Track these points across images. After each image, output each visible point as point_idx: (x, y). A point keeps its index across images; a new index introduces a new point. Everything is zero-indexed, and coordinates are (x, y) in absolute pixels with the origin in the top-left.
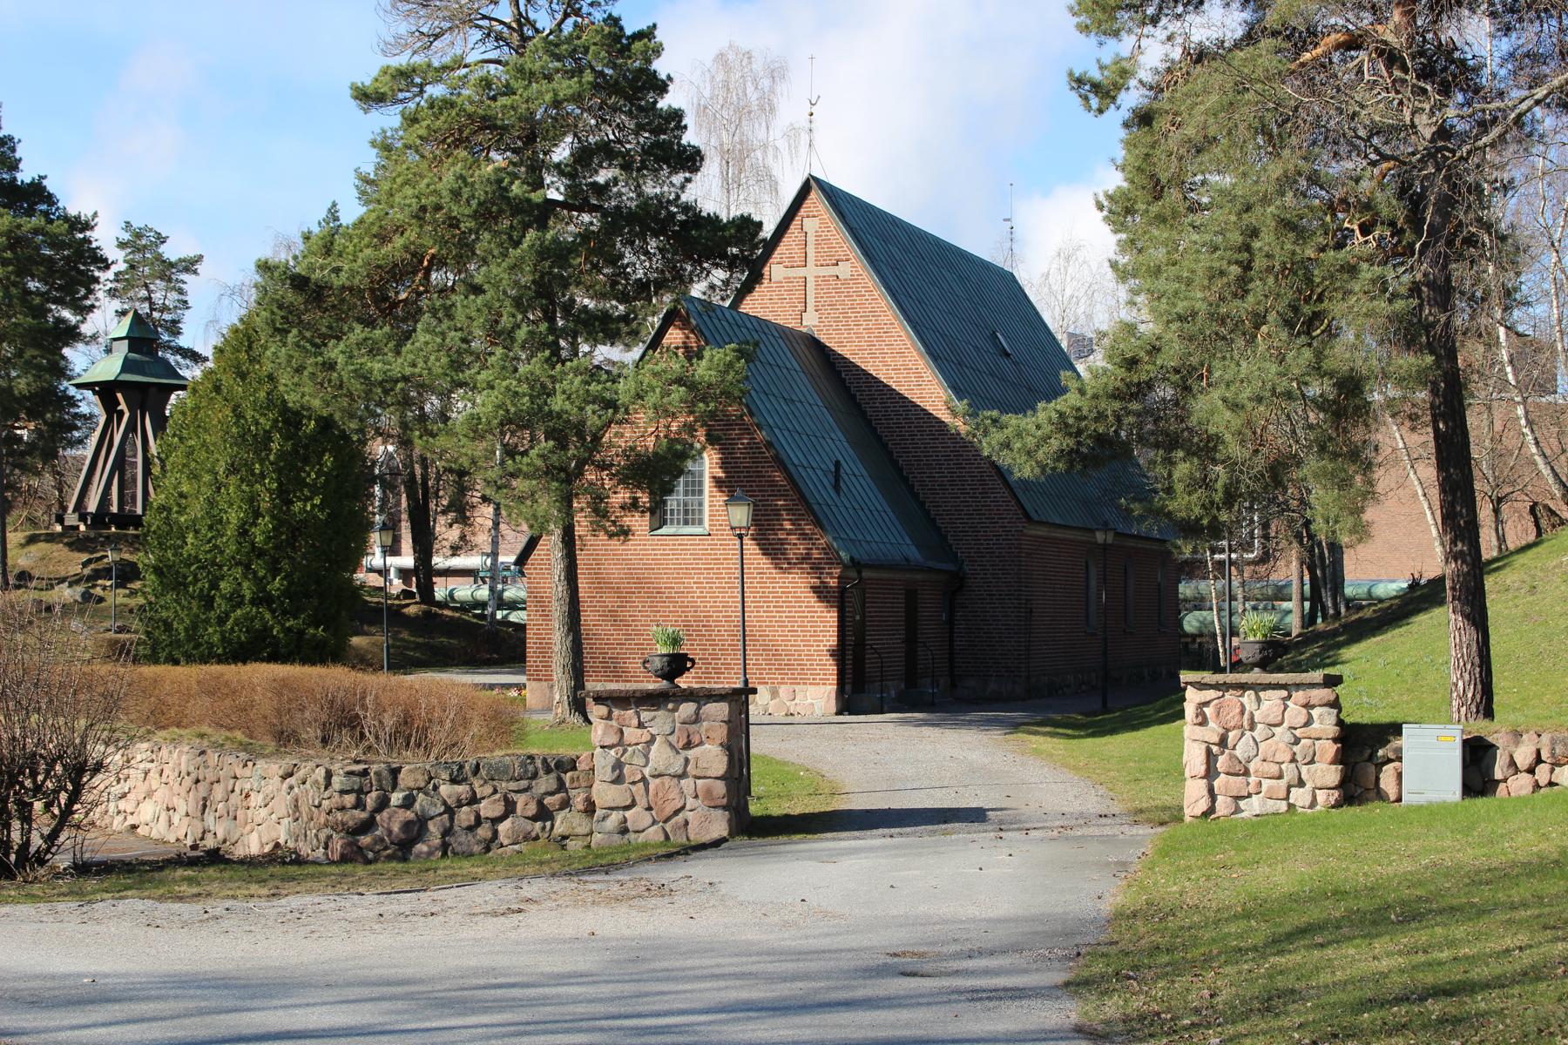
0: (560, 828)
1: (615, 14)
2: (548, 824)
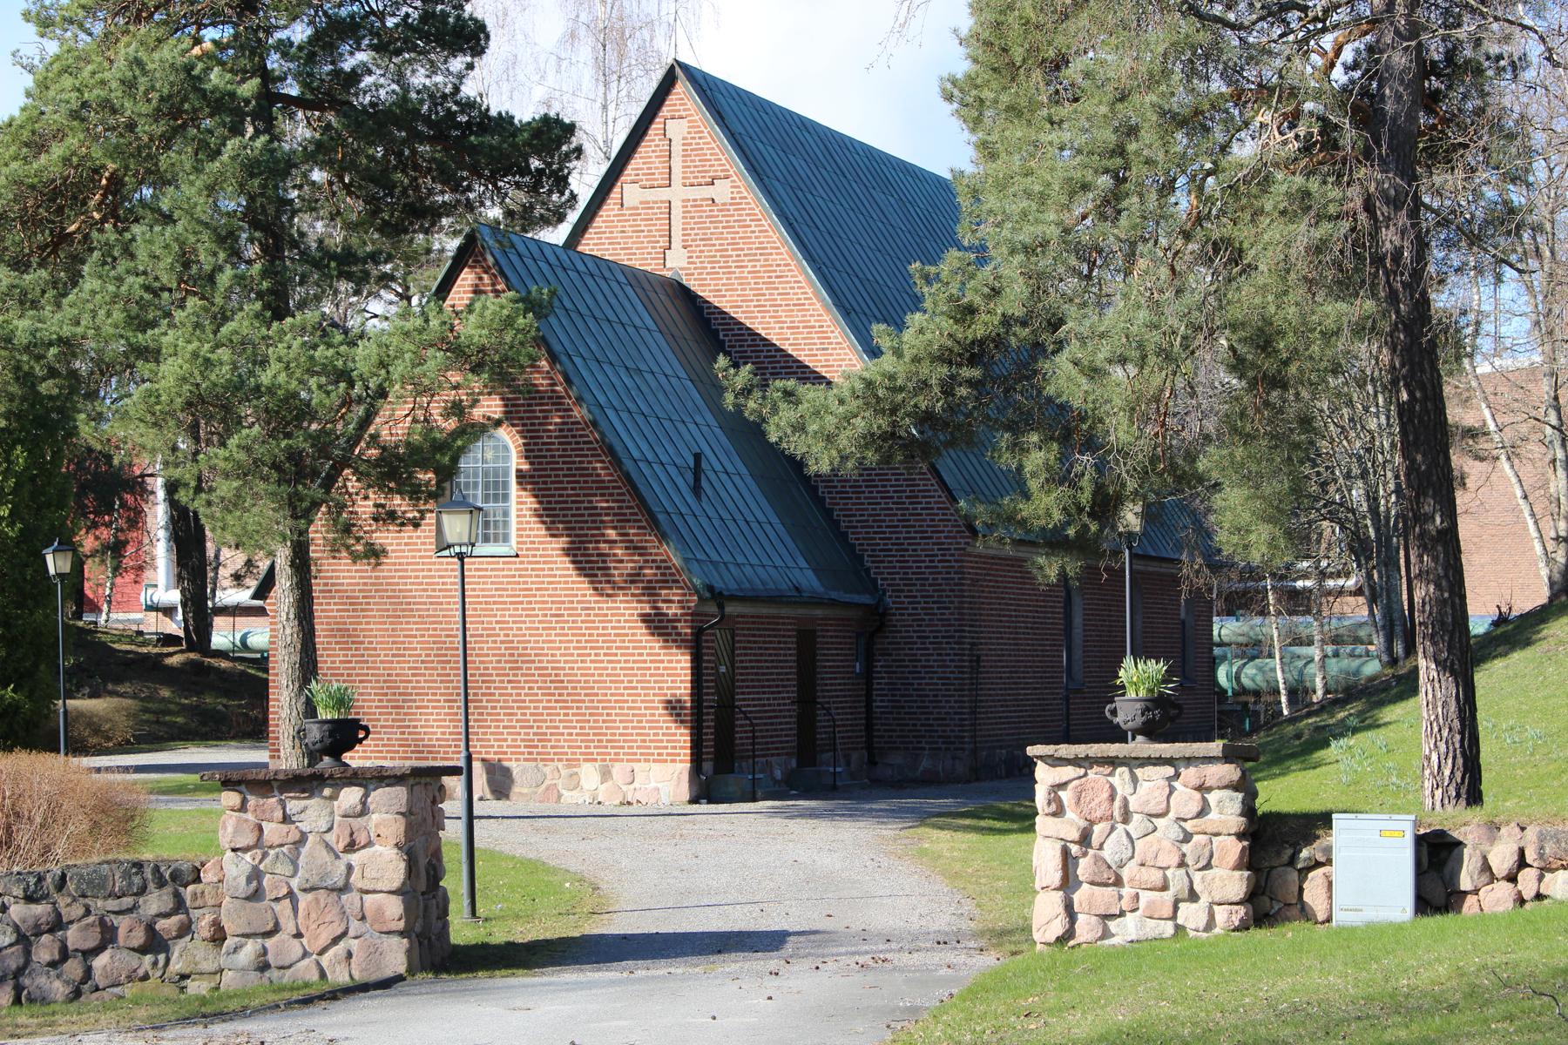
0: (176, 966)
2: (162, 957)
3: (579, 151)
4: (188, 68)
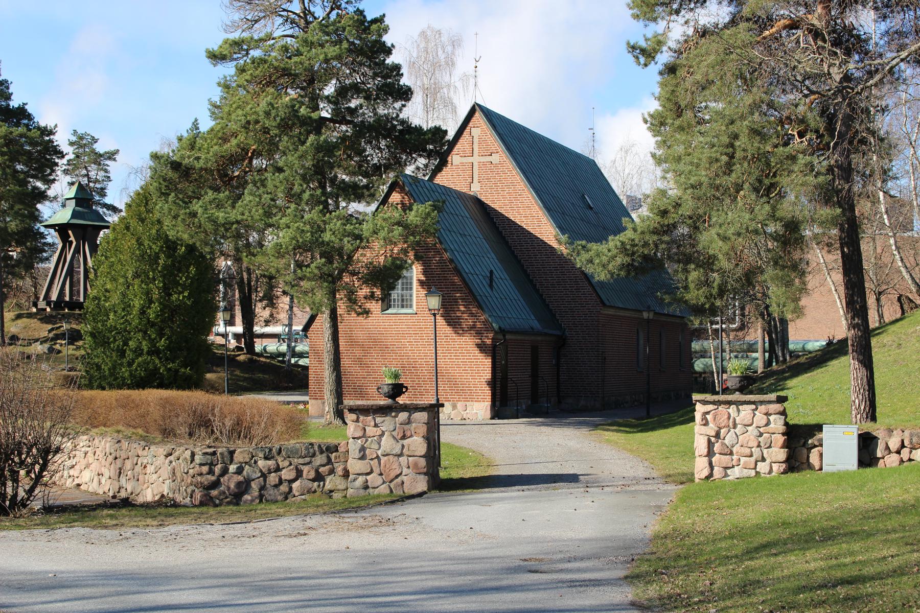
1: (361, 8)
2: (322, 483)
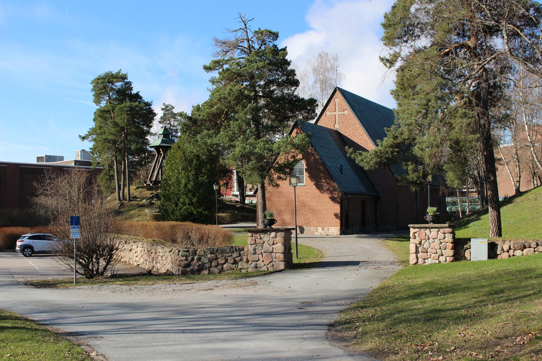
0: (240, 267)
1: (275, 44)
3: (317, 105)
4: (241, 90)
